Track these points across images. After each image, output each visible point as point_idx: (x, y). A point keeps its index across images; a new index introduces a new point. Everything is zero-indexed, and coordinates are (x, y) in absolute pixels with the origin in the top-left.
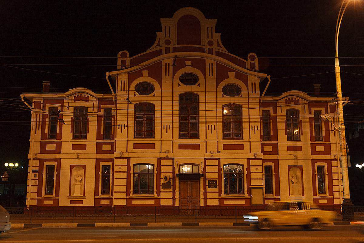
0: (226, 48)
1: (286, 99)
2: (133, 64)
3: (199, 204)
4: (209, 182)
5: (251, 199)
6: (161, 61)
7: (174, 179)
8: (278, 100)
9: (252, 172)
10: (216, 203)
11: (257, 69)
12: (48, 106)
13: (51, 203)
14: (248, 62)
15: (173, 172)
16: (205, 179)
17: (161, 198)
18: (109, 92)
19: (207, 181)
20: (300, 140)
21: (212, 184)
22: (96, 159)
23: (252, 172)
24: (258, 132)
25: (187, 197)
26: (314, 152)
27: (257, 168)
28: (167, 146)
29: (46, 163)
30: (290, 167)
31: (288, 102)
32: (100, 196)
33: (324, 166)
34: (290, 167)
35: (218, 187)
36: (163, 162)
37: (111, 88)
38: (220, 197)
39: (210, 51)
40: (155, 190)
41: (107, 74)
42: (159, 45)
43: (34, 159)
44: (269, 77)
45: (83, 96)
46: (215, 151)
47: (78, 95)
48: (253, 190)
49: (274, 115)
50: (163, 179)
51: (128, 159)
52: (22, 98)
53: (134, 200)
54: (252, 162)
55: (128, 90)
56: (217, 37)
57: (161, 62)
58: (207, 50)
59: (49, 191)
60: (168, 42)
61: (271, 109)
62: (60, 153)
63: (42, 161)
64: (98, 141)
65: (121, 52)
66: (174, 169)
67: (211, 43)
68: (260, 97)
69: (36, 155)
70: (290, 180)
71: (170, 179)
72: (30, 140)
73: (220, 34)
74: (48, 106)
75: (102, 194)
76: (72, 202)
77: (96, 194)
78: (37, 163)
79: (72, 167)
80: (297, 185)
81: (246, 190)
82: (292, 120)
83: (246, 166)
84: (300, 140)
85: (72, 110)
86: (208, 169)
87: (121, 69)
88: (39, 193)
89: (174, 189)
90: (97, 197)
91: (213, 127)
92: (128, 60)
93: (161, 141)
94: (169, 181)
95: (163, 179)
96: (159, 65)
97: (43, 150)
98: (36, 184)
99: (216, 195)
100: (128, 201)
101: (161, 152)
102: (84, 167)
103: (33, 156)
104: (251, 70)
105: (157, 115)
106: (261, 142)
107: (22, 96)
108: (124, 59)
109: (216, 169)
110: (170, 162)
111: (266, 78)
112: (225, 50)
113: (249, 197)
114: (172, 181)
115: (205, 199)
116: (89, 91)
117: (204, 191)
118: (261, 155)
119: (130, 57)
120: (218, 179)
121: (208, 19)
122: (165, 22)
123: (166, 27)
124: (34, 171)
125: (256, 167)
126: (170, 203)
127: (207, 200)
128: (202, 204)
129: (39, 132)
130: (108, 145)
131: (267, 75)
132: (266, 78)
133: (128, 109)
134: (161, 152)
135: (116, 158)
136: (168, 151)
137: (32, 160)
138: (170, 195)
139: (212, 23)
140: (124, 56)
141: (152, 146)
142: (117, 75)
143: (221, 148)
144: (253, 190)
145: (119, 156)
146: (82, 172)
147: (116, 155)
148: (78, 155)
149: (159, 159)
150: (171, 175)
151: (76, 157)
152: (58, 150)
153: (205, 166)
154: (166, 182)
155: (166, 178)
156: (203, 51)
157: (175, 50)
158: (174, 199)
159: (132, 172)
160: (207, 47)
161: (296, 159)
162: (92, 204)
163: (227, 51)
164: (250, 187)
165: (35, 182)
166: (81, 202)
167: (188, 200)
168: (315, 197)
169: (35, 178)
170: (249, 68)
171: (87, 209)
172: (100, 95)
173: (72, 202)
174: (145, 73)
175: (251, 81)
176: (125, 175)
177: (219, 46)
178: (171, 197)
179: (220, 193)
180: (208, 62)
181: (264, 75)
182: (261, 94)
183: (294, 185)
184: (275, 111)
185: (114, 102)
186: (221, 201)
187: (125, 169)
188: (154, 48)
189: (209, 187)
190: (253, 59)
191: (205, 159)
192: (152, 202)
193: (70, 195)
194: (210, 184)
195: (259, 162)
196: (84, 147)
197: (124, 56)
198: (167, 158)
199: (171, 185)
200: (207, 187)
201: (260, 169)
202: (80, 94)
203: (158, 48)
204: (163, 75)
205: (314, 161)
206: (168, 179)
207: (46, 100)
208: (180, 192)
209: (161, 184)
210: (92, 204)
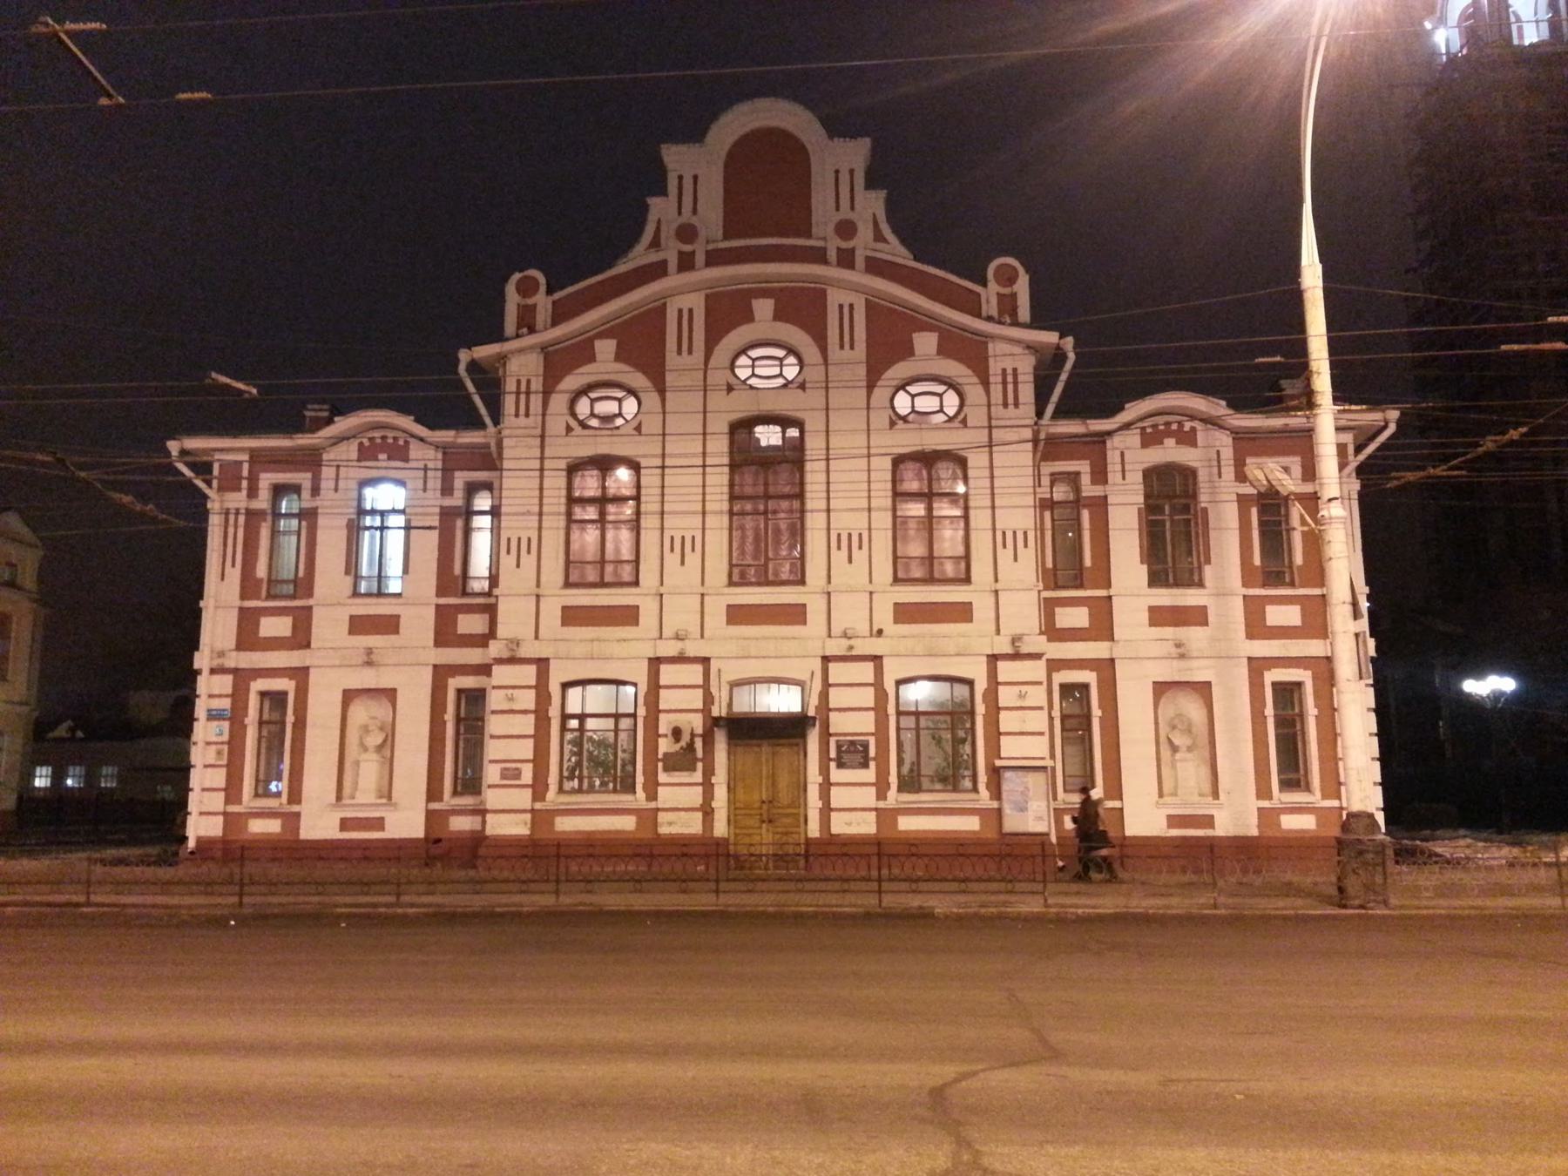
0: (903, 241)
1: (361, 444)
2: (558, 318)
3: (802, 829)
4: (839, 747)
5: (999, 811)
6: (663, 301)
7: (708, 738)
8: (1110, 433)
9: (1007, 708)
10: (865, 825)
11: (1024, 313)
12: (267, 480)
13: (273, 826)
14: (990, 295)
15: (706, 710)
16: (826, 734)
17: (658, 809)
18: (481, 425)
19: (833, 741)
20: (1201, 584)
21: (853, 753)
22: (435, 666)
23: (1007, 708)
24: (1028, 556)
25: (757, 805)
26: (1256, 627)
27: (1023, 693)
28: (682, 614)
29: (259, 685)
30: (1161, 689)
31: (1151, 439)
32: (448, 801)
33: (1299, 685)
34: (1161, 689)
35: (872, 764)
36: (668, 674)
37: (483, 411)
38: (881, 804)
39: (846, 259)
40: (640, 779)
41: (464, 356)
42: (655, 244)
43: (213, 671)
44: (1069, 343)
45: (390, 441)
46: (864, 628)
47: (371, 439)
48: (1008, 775)
49: (1097, 491)
50: (666, 736)
51: (542, 664)
52: (175, 453)
53: (904, 814)
54: (1006, 670)
55: (544, 415)
56: (872, 204)
57: (662, 310)
58: (832, 255)
59: (1294, 776)
60: (687, 233)
61: (1083, 467)
62: (308, 646)
63: (242, 678)
64: (443, 601)
65: (517, 276)
66: (708, 699)
67: (846, 229)
68: (1036, 424)
69: (221, 654)
70: (1163, 739)
71: (693, 735)
72: (202, 604)
73: (883, 194)
74: (267, 480)
75: (455, 793)
76: (345, 824)
77: (433, 793)
78: (225, 683)
79: (349, 696)
80: (1189, 756)
81: (982, 778)
82: (1167, 508)
83: (981, 686)
84: (1201, 584)
85: (1135, 478)
86: (837, 698)
87: (518, 336)
88: (232, 791)
89: (709, 772)
90: (435, 806)
91: (855, 539)
92: (543, 303)
93: (661, 595)
94: (690, 747)
95: (666, 736)
96: (655, 316)
97: (247, 638)
98: (222, 759)
99: (868, 797)
100: (541, 818)
101: (661, 638)
102: (390, 694)
103: (212, 659)
104: (1000, 323)
105: (882, 494)
106: (1039, 592)
107: (173, 446)
108: (530, 301)
109: (867, 697)
110: (693, 674)
111: (1058, 347)
112: (903, 250)
113: (995, 805)
114: (699, 744)
115: (827, 810)
116: (406, 422)
117: (820, 780)
118: (1037, 643)
119: (550, 291)
120: (872, 734)
121: (836, 139)
122: (676, 158)
123: (680, 178)
124: (213, 716)
125: (506, 691)
126: (691, 825)
127: (832, 814)
128: (814, 830)
129: (234, 574)
130: (477, 616)
131: (1060, 338)
132: (1058, 347)
133: (704, 470)
134: (661, 638)
135: (500, 661)
136: (683, 633)
137: (205, 672)
138: (695, 796)
139: (854, 154)
140: (527, 288)
141: (796, 614)
142: (503, 358)
143: (885, 617)
144: (1008, 775)
145: (506, 655)
146: (380, 710)
147: (495, 649)
148: (369, 651)
149: (655, 663)
150: (697, 723)
151: (362, 658)
152: (301, 638)
153: (826, 685)
154: (677, 747)
155: (677, 733)
156: (819, 256)
157: (715, 258)
158: (707, 812)
159: (554, 712)
160: (833, 245)
161: (1182, 656)
162: (420, 833)
163: (912, 257)
164: (998, 763)
165: (219, 753)
166: (1209, 821)
167: (763, 811)
168: (1265, 804)
169: (220, 739)
170: (994, 313)
171: (397, 851)
172: (446, 436)
173: (345, 824)
174: (606, 348)
175: (1000, 365)
176: (527, 724)
177: (879, 237)
178: (699, 801)
179: (881, 788)
180: (835, 297)
181: (1051, 337)
182: (1040, 414)
183: (1178, 756)
184: (1100, 475)
185: (489, 460)
186: (886, 817)
187: (528, 699)
188: (639, 256)
189: (840, 765)
190: (1008, 278)
191: (826, 659)
192: (627, 823)
193: (339, 798)
194: (843, 752)
195: (1037, 670)
196: (1197, 616)
197: (527, 288)
198: (681, 659)
199: (659, 760)
200: (833, 765)
201: (1038, 696)
202: (377, 434)
203: (654, 257)
204: (668, 354)
205: (1257, 666)
206: (686, 738)
207: (260, 460)
208: (732, 786)
209: (660, 756)
210: (420, 833)
